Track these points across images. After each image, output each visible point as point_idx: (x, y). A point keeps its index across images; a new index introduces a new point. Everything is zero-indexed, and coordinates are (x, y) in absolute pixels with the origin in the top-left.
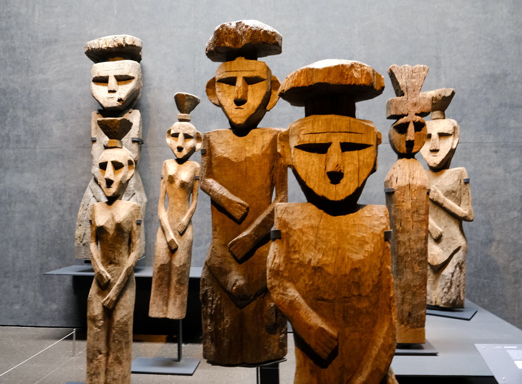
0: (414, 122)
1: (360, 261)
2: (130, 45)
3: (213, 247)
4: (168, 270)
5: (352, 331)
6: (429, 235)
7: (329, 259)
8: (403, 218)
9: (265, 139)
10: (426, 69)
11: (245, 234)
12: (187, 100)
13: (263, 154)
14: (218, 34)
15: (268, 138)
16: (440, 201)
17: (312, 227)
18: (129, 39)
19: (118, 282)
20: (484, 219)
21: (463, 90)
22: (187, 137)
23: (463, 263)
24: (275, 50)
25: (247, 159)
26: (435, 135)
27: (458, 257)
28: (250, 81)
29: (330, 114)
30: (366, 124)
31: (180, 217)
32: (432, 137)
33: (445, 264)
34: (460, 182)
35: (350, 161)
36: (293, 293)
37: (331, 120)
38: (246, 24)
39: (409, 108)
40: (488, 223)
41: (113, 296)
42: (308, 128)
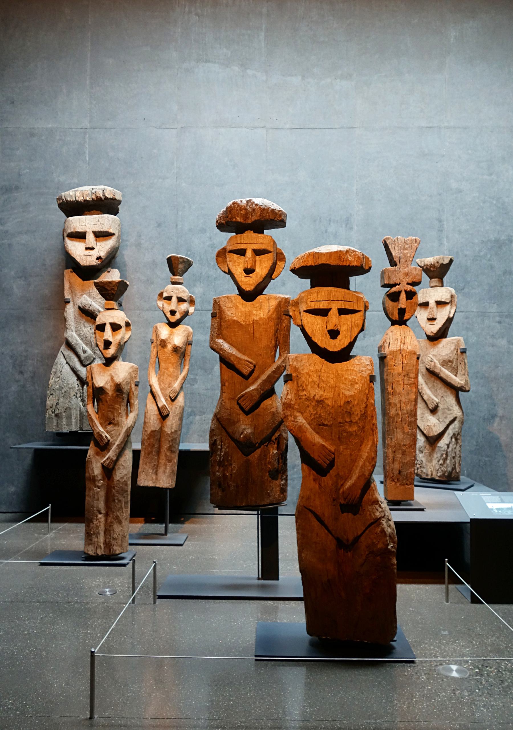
0: (406, 291)
1: (351, 396)
2: (110, 199)
4: (158, 437)
5: (345, 448)
6: (419, 400)
8: (394, 381)
9: (271, 304)
10: (418, 241)
11: (252, 388)
12: (181, 263)
13: (269, 318)
14: (229, 210)
15: (274, 303)
16: (437, 371)
17: (316, 371)
18: (109, 192)
19: (117, 443)
20: (487, 393)
21: (466, 256)
22: (180, 300)
23: (458, 434)
25: (255, 322)
26: (432, 303)
27: (454, 428)
28: (258, 252)
29: (330, 286)
30: (357, 295)
31: (172, 383)
32: (430, 305)
33: (441, 435)
34: (457, 351)
35: (345, 322)
36: (301, 420)
37: (331, 291)
38: (256, 203)
39: (401, 278)
40: (491, 397)
41: (113, 456)
42: (314, 297)
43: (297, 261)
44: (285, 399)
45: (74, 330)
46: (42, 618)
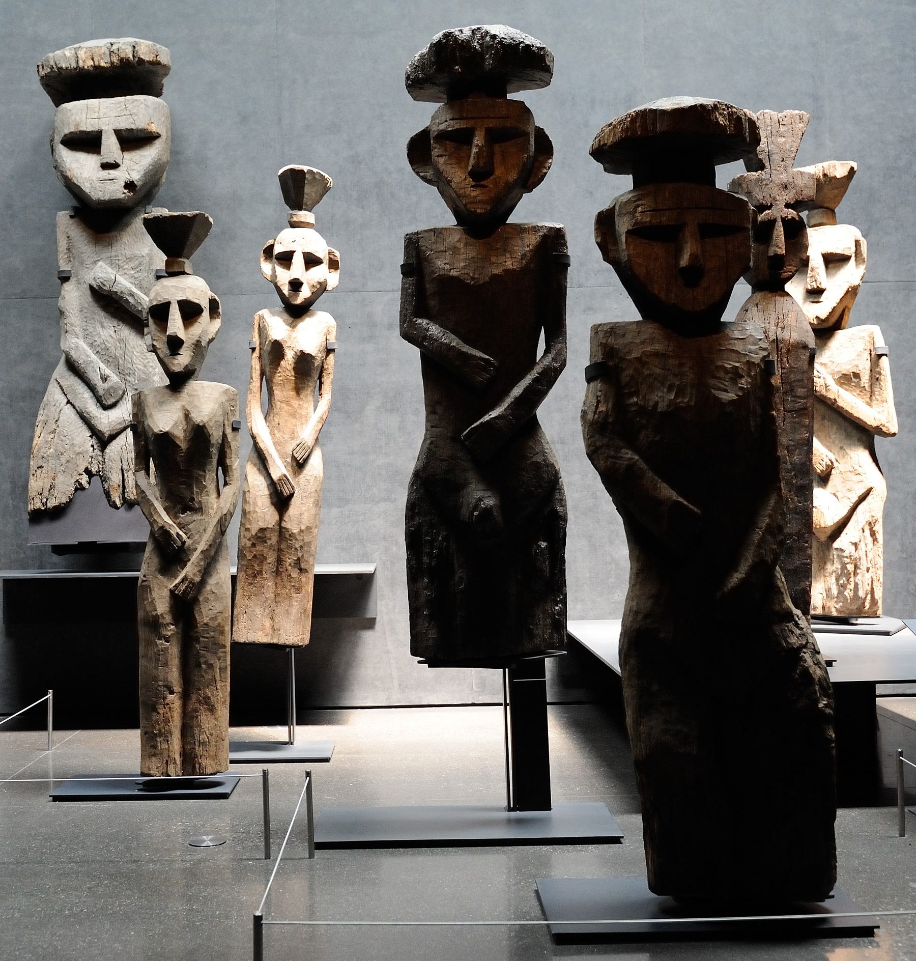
0: (783, 219)
2: (149, 62)
3: (431, 443)
7: (686, 400)
10: (805, 119)
11: (494, 414)
18: (146, 50)
19: (201, 547)
21: (869, 168)
24: (541, 80)
38: (493, 32)
41: (195, 575)
43: (610, 131)
44: (595, 413)
45: (81, 334)
46: (90, 888)
